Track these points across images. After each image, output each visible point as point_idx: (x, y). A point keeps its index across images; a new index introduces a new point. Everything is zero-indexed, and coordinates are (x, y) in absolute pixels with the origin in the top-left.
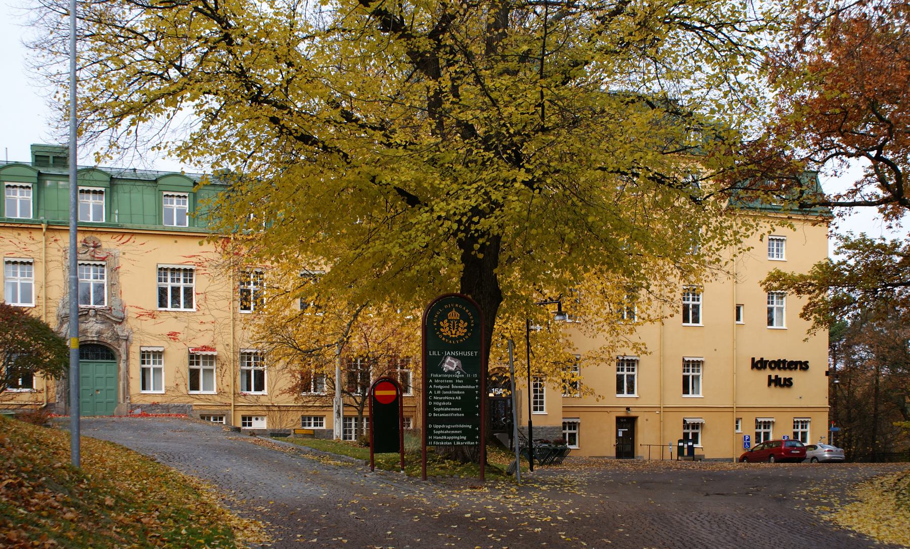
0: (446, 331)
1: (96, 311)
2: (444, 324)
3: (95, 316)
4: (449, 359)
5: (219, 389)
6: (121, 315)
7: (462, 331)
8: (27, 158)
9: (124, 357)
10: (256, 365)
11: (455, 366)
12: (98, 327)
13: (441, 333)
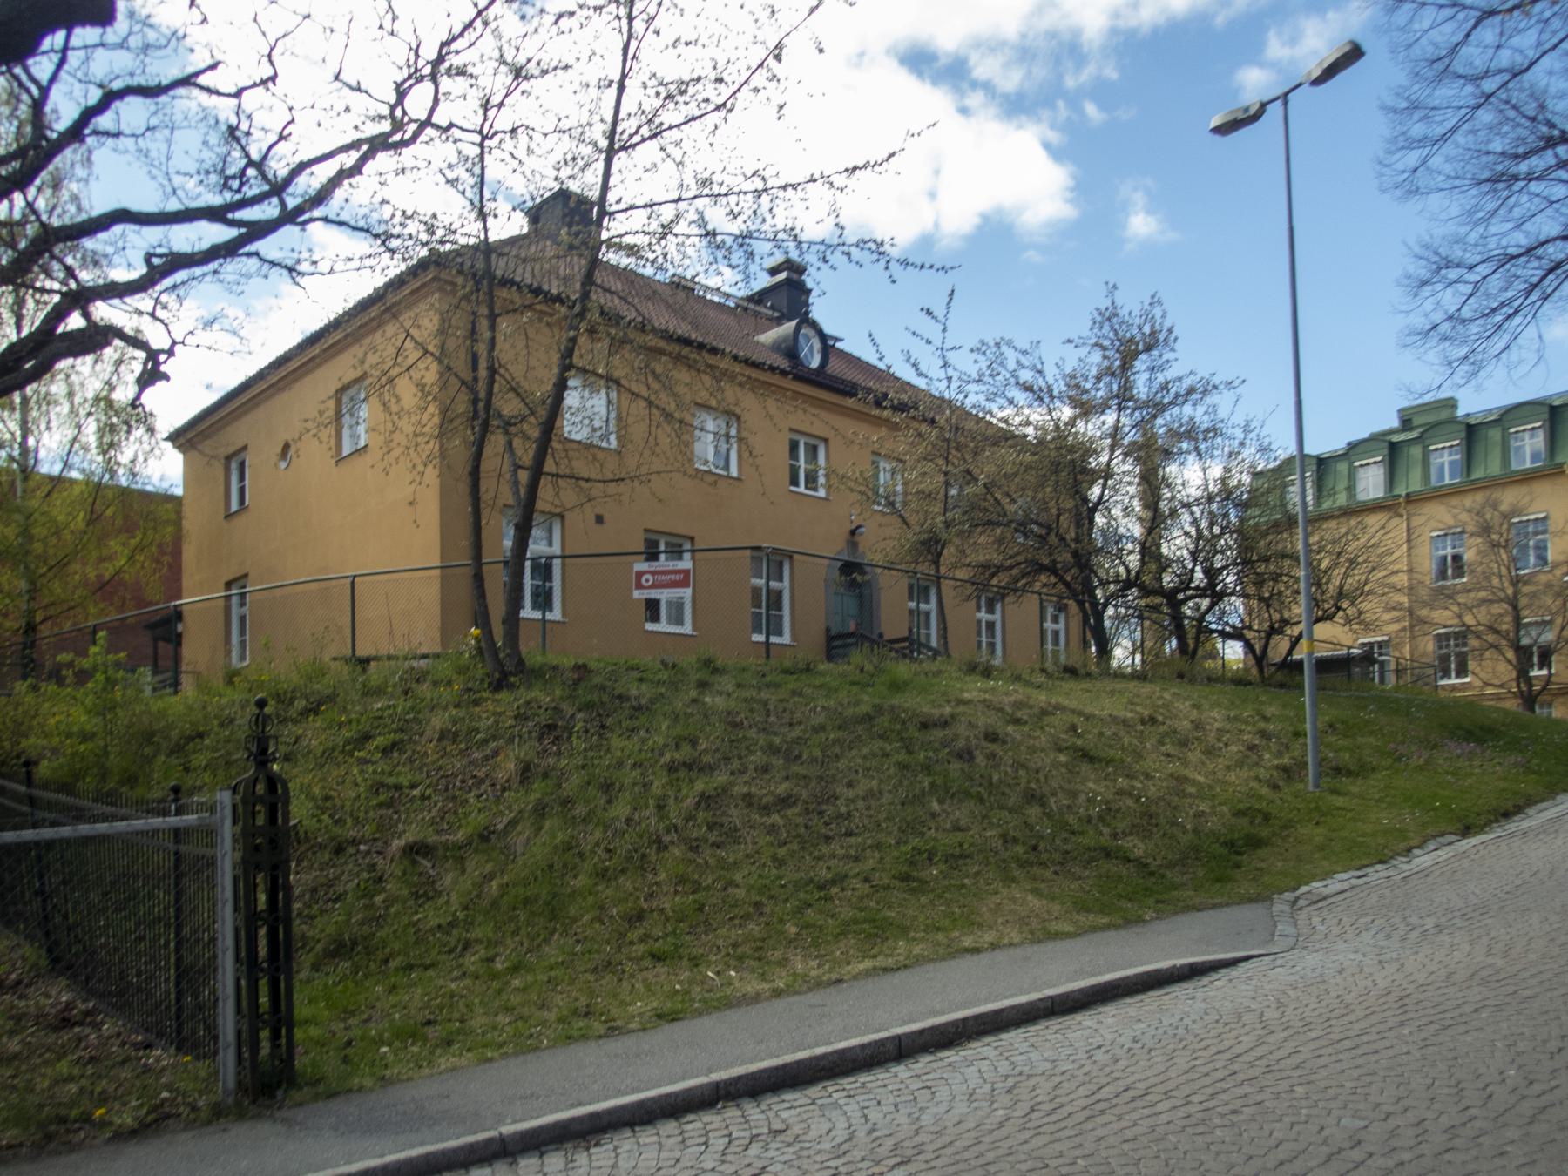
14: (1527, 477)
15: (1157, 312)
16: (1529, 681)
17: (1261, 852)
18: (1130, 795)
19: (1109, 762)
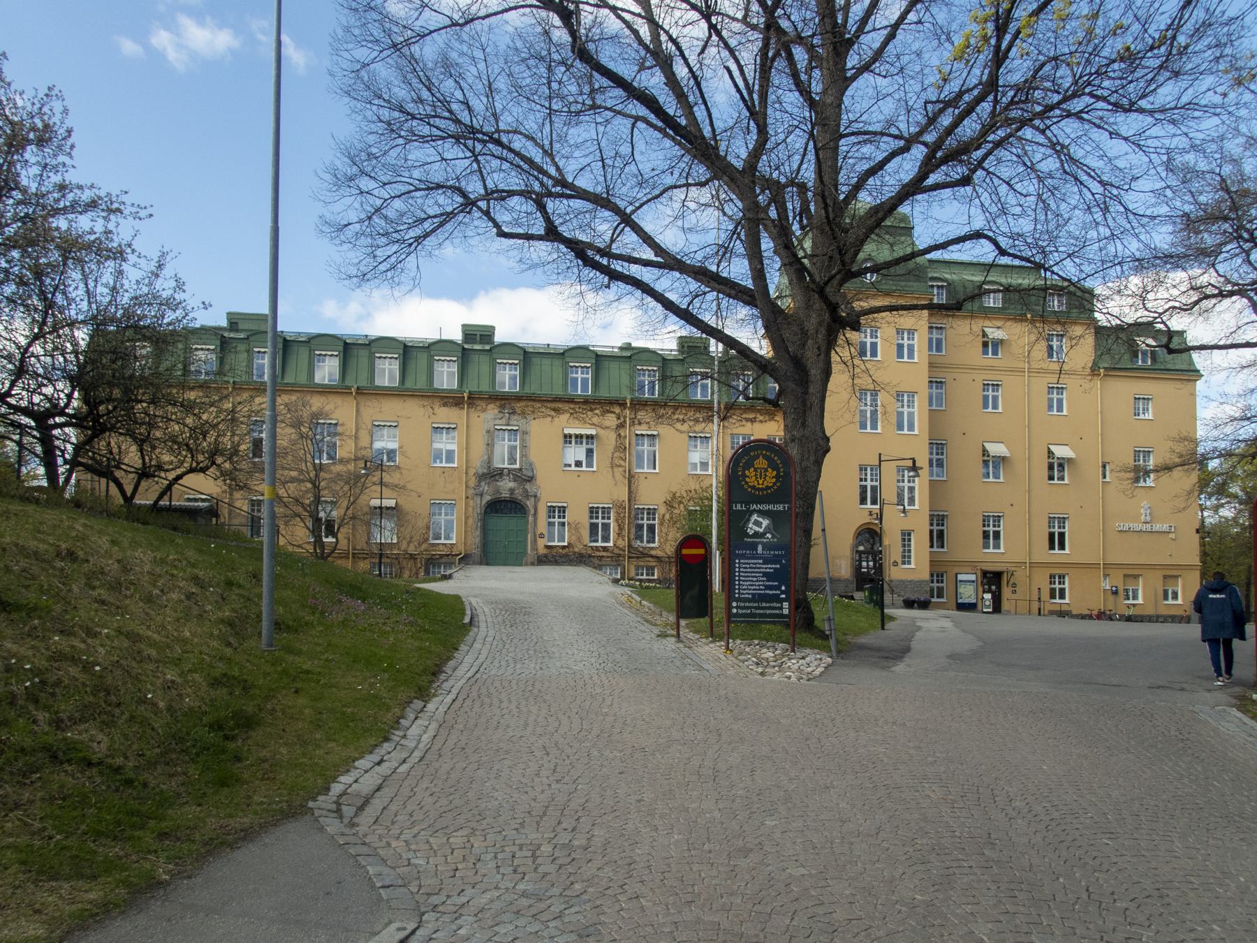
0: (752, 481)
1: (510, 470)
2: (750, 473)
3: (508, 475)
4: (755, 517)
5: (569, 544)
6: (530, 474)
7: (770, 481)
8: (457, 336)
9: (532, 512)
10: (446, 514)
11: (764, 526)
12: (511, 485)
13: (747, 483)
14: (325, 390)
15: (57, 106)
16: (322, 545)
17: (258, 734)
18: (74, 660)
19: (32, 611)
